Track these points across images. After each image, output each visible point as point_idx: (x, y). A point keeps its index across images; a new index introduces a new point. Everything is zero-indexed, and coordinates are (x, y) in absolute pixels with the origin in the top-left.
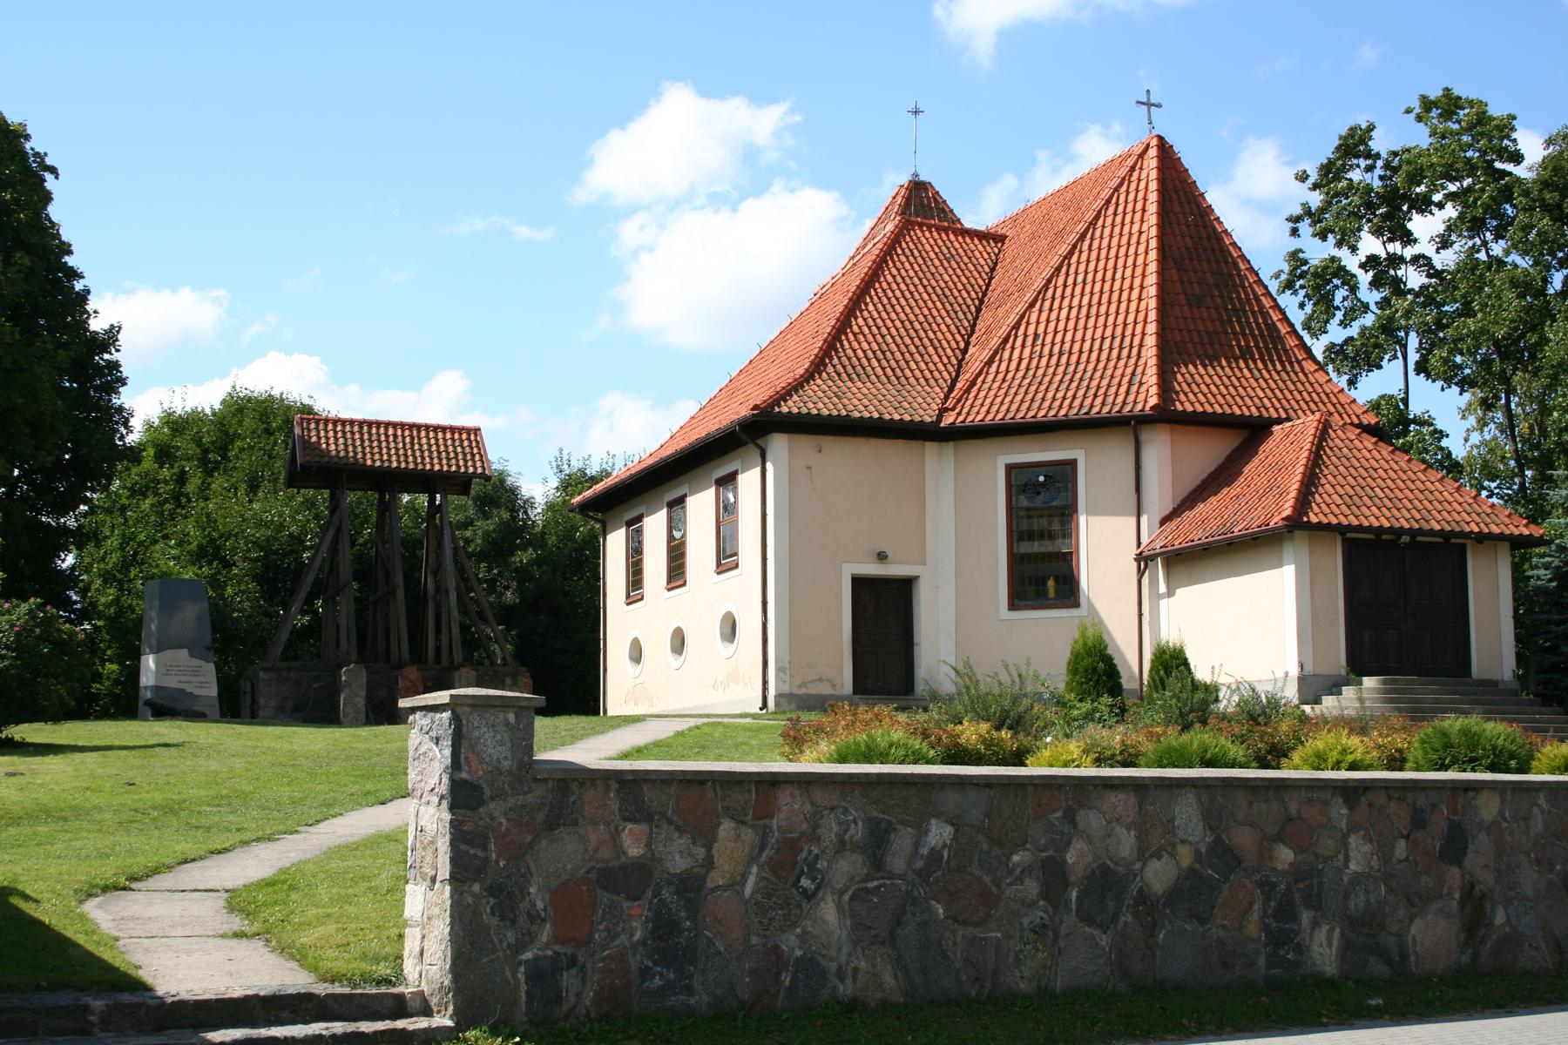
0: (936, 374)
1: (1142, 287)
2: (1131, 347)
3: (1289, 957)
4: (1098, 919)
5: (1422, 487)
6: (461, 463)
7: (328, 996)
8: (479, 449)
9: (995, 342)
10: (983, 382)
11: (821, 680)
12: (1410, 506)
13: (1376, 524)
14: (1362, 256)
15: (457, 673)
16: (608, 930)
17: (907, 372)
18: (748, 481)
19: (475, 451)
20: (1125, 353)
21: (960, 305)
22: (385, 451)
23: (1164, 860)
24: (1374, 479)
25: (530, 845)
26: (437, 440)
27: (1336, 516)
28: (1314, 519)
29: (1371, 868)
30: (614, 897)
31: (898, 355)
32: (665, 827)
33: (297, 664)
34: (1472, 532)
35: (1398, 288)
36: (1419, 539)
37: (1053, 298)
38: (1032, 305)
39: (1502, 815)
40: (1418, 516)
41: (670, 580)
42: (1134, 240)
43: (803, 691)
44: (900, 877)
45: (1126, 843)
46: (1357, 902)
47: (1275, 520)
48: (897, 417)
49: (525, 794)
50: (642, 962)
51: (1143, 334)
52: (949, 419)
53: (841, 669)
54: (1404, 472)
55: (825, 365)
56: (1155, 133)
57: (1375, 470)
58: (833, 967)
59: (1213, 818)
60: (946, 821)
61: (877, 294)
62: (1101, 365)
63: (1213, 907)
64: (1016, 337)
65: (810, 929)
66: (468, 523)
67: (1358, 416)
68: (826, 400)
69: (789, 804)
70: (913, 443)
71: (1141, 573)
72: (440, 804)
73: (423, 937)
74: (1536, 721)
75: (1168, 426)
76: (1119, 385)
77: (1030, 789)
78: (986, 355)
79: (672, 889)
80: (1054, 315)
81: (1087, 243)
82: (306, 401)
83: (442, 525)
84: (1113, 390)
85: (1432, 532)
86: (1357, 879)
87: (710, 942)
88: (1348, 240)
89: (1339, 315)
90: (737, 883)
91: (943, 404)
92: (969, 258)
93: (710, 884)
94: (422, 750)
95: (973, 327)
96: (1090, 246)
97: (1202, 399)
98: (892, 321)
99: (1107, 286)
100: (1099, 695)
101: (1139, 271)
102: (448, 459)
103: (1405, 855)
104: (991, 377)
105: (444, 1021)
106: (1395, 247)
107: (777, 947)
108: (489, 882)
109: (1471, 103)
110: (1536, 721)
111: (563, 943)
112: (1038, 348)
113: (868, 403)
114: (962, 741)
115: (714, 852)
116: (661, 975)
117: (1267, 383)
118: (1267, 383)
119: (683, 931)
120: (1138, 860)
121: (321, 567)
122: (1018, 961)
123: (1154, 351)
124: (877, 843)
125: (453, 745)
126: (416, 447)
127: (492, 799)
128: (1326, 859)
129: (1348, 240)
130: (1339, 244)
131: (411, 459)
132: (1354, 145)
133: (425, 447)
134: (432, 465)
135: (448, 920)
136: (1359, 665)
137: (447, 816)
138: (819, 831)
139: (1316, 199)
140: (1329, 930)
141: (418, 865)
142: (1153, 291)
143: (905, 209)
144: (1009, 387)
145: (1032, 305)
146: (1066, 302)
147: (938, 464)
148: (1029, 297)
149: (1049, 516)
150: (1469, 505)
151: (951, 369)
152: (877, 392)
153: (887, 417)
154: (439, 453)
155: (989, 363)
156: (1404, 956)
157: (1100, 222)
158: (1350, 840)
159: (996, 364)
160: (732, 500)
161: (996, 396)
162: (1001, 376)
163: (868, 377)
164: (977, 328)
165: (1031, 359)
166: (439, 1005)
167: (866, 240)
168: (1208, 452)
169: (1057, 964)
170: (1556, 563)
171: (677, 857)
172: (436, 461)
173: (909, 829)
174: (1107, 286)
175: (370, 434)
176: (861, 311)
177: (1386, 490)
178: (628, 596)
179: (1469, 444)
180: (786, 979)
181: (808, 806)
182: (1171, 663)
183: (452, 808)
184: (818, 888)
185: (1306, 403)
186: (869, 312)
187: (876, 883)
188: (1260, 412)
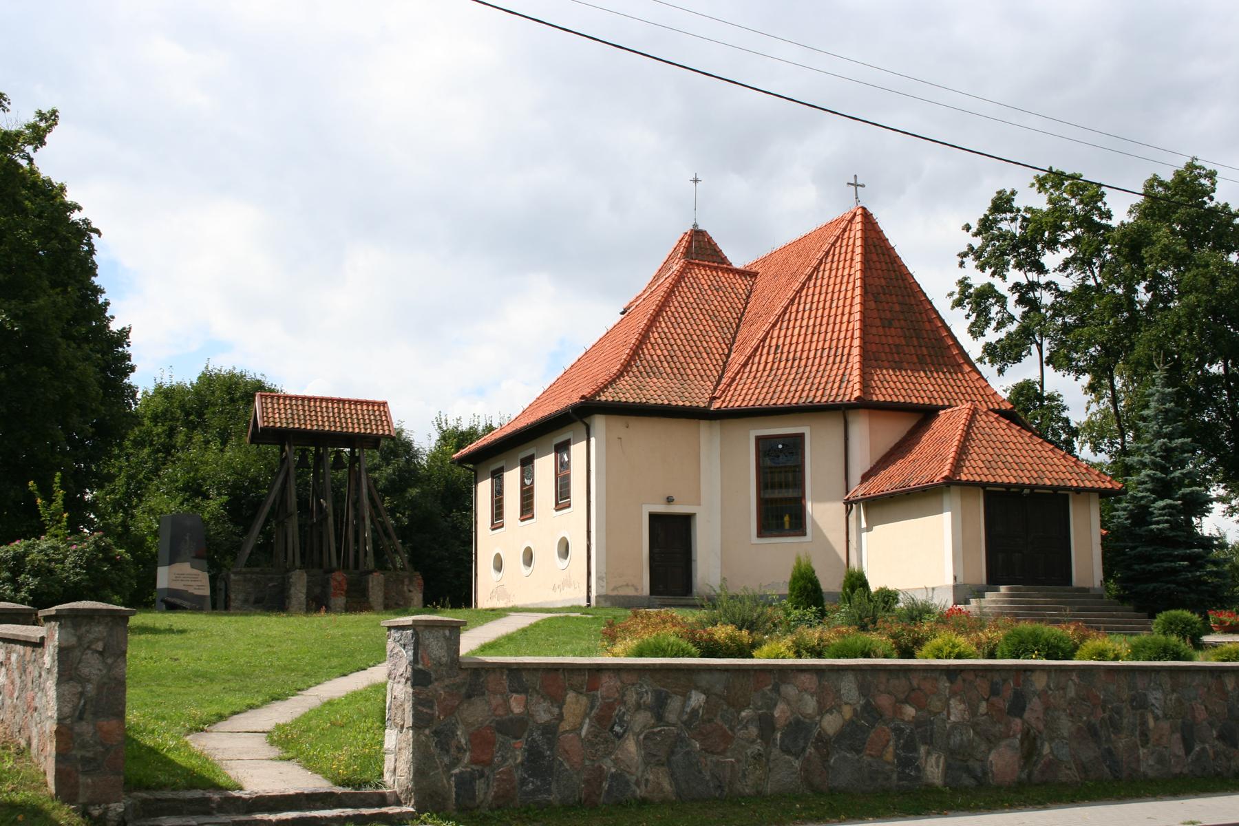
0: (708, 372)
1: (850, 314)
2: (842, 355)
3: (912, 773)
4: (793, 751)
5: (1039, 455)
6: (374, 427)
7: (342, 794)
8: (387, 417)
9: (749, 351)
10: (741, 379)
11: (627, 585)
12: (1030, 468)
13: (1006, 481)
14: (1010, 283)
15: (371, 576)
16: (502, 756)
17: (688, 371)
18: (577, 450)
19: (384, 418)
20: (838, 359)
21: (725, 323)
22: (320, 418)
23: (834, 715)
24: (1006, 450)
25: (457, 707)
26: (357, 410)
27: (979, 475)
28: (964, 478)
29: (964, 719)
30: (507, 738)
31: (682, 359)
32: (536, 696)
33: (258, 569)
34: (1072, 486)
35: (1034, 305)
36: (1036, 491)
37: (789, 320)
38: (774, 325)
39: (1048, 686)
40: (1035, 476)
41: (522, 514)
42: (845, 280)
43: (615, 593)
44: (673, 725)
45: (810, 705)
46: (955, 740)
47: (938, 479)
48: (680, 403)
49: (455, 677)
50: (522, 775)
51: (851, 346)
52: (716, 405)
53: (642, 578)
54: (1027, 444)
55: (631, 366)
56: (860, 205)
57: (1007, 443)
58: (634, 778)
59: (864, 690)
60: (701, 692)
61: (667, 315)
62: (822, 368)
63: (865, 744)
64: (763, 347)
65: (620, 756)
66: (376, 468)
67: (998, 404)
68: (632, 392)
69: (608, 683)
70: (692, 421)
71: (848, 512)
72: (406, 682)
73: (396, 760)
74: (1113, 616)
75: (867, 411)
76: (834, 382)
77: (752, 673)
78: (742, 359)
79: (539, 732)
80: (789, 333)
81: (813, 281)
82: (259, 377)
83: (360, 471)
84: (829, 386)
85: (1044, 487)
86: (955, 726)
87: (561, 764)
88: (1000, 271)
89: (994, 324)
90: (576, 729)
91: (713, 394)
92: (732, 289)
93: (561, 729)
94: (395, 651)
95: (734, 338)
96: (815, 284)
97: (891, 392)
98: (678, 335)
99: (826, 312)
100: (809, 606)
101: (848, 302)
102: (365, 424)
103: (985, 711)
104: (746, 375)
105: (409, 808)
106: (1033, 276)
107: (601, 767)
108: (434, 728)
109: (1073, 177)
110: (1113, 616)
111: (476, 764)
112: (778, 355)
113: (661, 393)
114: (716, 637)
115: (564, 710)
116: (532, 782)
117: (936, 381)
118: (936, 381)
119: (545, 757)
120: (819, 714)
121: (275, 500)
122: (744, 776)
123: (857, 359)
124: (658, 708)
125: (414, 649)
126: (342, 415)
127: (436, 680)
128: (936, 714)
129: (1000, 271)
130: (993, 274)
131: (338, 424)
132: (1002, 203)
133: (348, 416)
134: (354, 428)
135: (411, 750)
136: (994, 580)
137: (411, 690)
138: (625, 698)
139: (977, 242)
140: (936, 758)
141: (392, 718)
142: (857, 316)
143: (687, 253)
144: (758, 382)
145: (774, 325)
146: (798, 323)
147: (709, 438)
148: (772, 319)
149: (786, 472)
150: (1071, 467)
151: (718, 368)
152: (667, 386)
153: (674, 403)
154: (358, 420)
155: (745, 365)
156: (985, 773)
157: (822, 268)
158: (951, 702)
159: (749, 366)
160: (566, 459)
161: (749, 389)
162: (753, 375)
163: (661, 374)
164: (737, 339)
165: (774, 362)
166: (406, 799)
167: (656, 278)
168: (893, 430)
169: (768, 778)
170: (1131, 507)
171: (542, 713)
172: (356, 425)
173: (679, 697)
174: (826, 312)
175: (309, 406)
176: (657, 328)
177: (1014, 457)
178: (557, 504)
179: (1090, 412)
180: (605, 785)
181: (619, 683)
182: (857, 582)
183: (413, 686)
184: (625, 732)
185: (963, 394)
186: (662, 328)
187: (659, 729)
188: (931, 401)
